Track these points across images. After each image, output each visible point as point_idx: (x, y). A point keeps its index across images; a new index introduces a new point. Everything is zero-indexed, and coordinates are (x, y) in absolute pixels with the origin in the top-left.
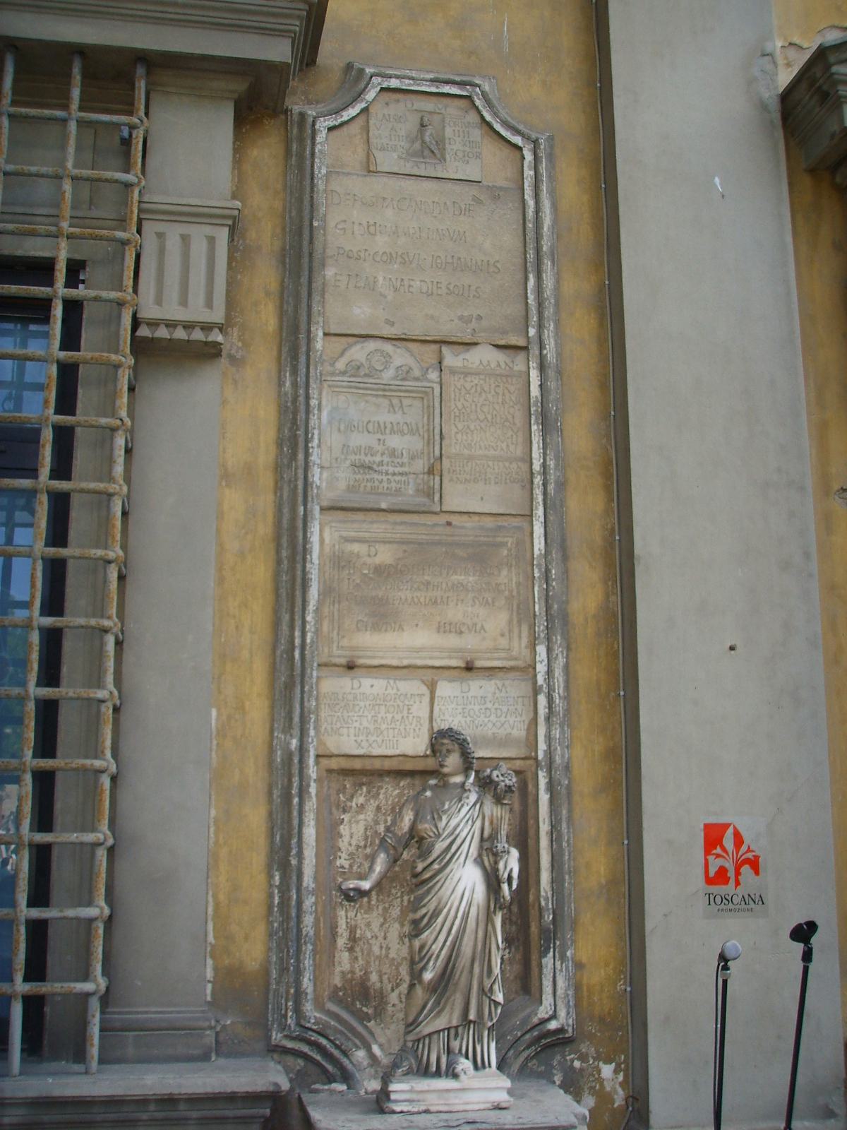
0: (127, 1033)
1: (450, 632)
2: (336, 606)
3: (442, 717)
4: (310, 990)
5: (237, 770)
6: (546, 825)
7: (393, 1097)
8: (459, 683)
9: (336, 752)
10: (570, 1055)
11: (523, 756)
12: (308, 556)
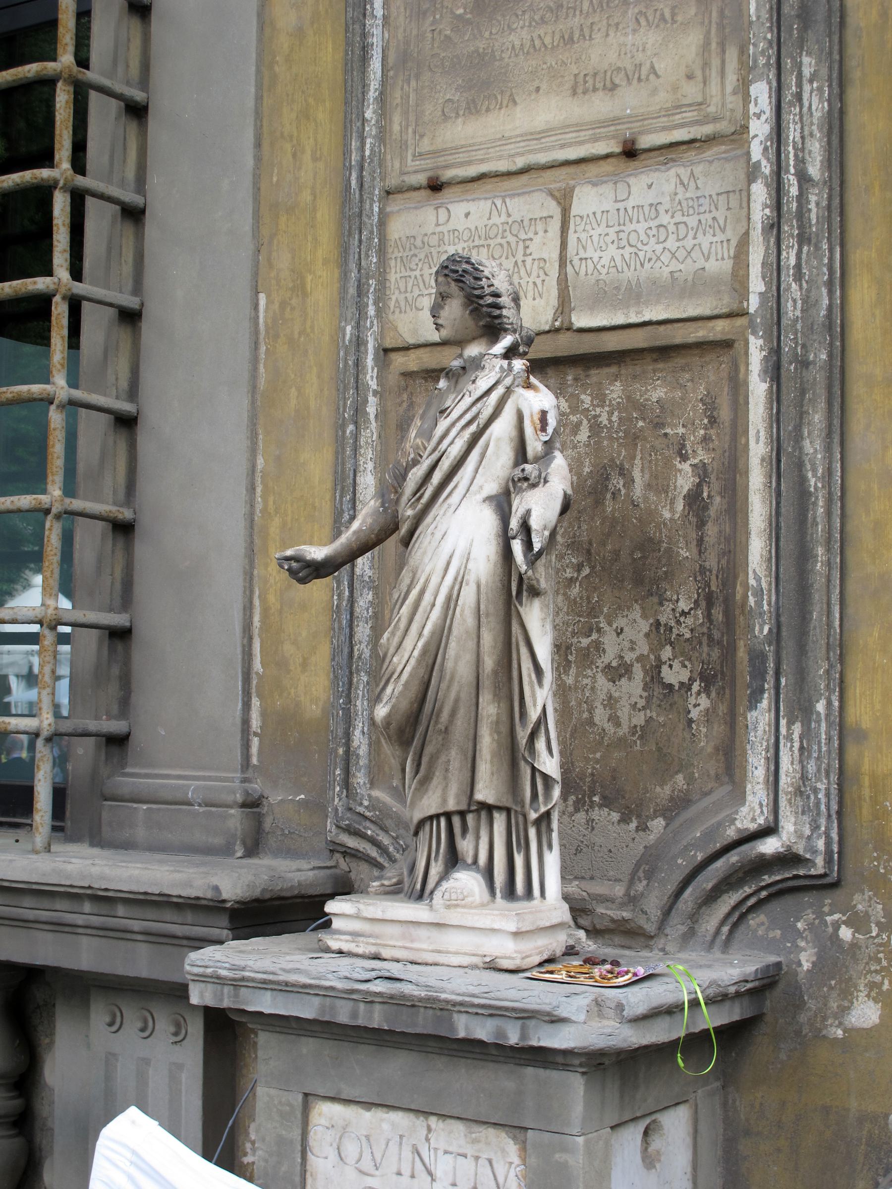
0: (140, 805)
1: (595, 90)
2: (413, 83)
3: (582, 255)
4: (363, 751)
5: (293, 390)
6: (761, 444)
7: (336, 924)
8: (611, 185)
9: (412, 341)
10: (831, 914)
11: (725, 310)
12: (368, 7)
